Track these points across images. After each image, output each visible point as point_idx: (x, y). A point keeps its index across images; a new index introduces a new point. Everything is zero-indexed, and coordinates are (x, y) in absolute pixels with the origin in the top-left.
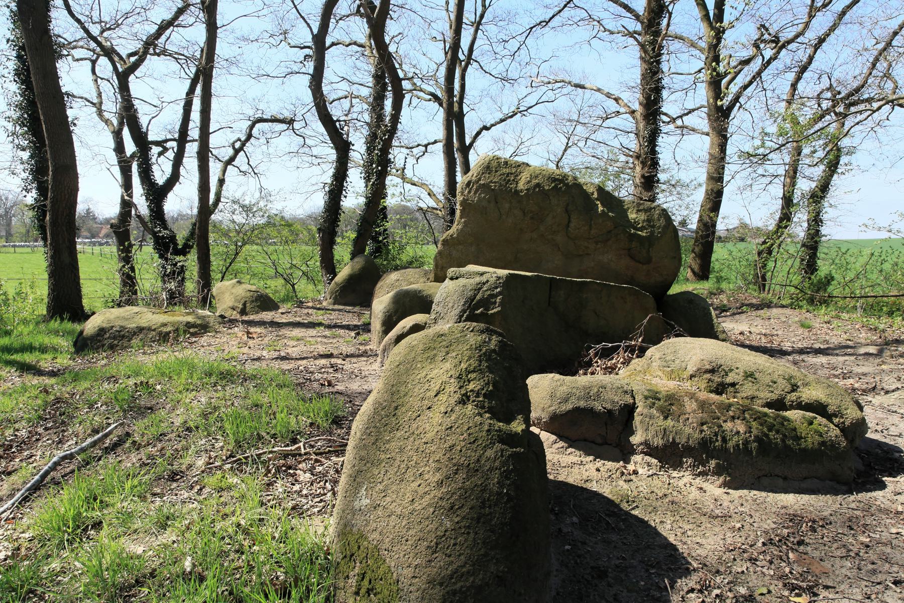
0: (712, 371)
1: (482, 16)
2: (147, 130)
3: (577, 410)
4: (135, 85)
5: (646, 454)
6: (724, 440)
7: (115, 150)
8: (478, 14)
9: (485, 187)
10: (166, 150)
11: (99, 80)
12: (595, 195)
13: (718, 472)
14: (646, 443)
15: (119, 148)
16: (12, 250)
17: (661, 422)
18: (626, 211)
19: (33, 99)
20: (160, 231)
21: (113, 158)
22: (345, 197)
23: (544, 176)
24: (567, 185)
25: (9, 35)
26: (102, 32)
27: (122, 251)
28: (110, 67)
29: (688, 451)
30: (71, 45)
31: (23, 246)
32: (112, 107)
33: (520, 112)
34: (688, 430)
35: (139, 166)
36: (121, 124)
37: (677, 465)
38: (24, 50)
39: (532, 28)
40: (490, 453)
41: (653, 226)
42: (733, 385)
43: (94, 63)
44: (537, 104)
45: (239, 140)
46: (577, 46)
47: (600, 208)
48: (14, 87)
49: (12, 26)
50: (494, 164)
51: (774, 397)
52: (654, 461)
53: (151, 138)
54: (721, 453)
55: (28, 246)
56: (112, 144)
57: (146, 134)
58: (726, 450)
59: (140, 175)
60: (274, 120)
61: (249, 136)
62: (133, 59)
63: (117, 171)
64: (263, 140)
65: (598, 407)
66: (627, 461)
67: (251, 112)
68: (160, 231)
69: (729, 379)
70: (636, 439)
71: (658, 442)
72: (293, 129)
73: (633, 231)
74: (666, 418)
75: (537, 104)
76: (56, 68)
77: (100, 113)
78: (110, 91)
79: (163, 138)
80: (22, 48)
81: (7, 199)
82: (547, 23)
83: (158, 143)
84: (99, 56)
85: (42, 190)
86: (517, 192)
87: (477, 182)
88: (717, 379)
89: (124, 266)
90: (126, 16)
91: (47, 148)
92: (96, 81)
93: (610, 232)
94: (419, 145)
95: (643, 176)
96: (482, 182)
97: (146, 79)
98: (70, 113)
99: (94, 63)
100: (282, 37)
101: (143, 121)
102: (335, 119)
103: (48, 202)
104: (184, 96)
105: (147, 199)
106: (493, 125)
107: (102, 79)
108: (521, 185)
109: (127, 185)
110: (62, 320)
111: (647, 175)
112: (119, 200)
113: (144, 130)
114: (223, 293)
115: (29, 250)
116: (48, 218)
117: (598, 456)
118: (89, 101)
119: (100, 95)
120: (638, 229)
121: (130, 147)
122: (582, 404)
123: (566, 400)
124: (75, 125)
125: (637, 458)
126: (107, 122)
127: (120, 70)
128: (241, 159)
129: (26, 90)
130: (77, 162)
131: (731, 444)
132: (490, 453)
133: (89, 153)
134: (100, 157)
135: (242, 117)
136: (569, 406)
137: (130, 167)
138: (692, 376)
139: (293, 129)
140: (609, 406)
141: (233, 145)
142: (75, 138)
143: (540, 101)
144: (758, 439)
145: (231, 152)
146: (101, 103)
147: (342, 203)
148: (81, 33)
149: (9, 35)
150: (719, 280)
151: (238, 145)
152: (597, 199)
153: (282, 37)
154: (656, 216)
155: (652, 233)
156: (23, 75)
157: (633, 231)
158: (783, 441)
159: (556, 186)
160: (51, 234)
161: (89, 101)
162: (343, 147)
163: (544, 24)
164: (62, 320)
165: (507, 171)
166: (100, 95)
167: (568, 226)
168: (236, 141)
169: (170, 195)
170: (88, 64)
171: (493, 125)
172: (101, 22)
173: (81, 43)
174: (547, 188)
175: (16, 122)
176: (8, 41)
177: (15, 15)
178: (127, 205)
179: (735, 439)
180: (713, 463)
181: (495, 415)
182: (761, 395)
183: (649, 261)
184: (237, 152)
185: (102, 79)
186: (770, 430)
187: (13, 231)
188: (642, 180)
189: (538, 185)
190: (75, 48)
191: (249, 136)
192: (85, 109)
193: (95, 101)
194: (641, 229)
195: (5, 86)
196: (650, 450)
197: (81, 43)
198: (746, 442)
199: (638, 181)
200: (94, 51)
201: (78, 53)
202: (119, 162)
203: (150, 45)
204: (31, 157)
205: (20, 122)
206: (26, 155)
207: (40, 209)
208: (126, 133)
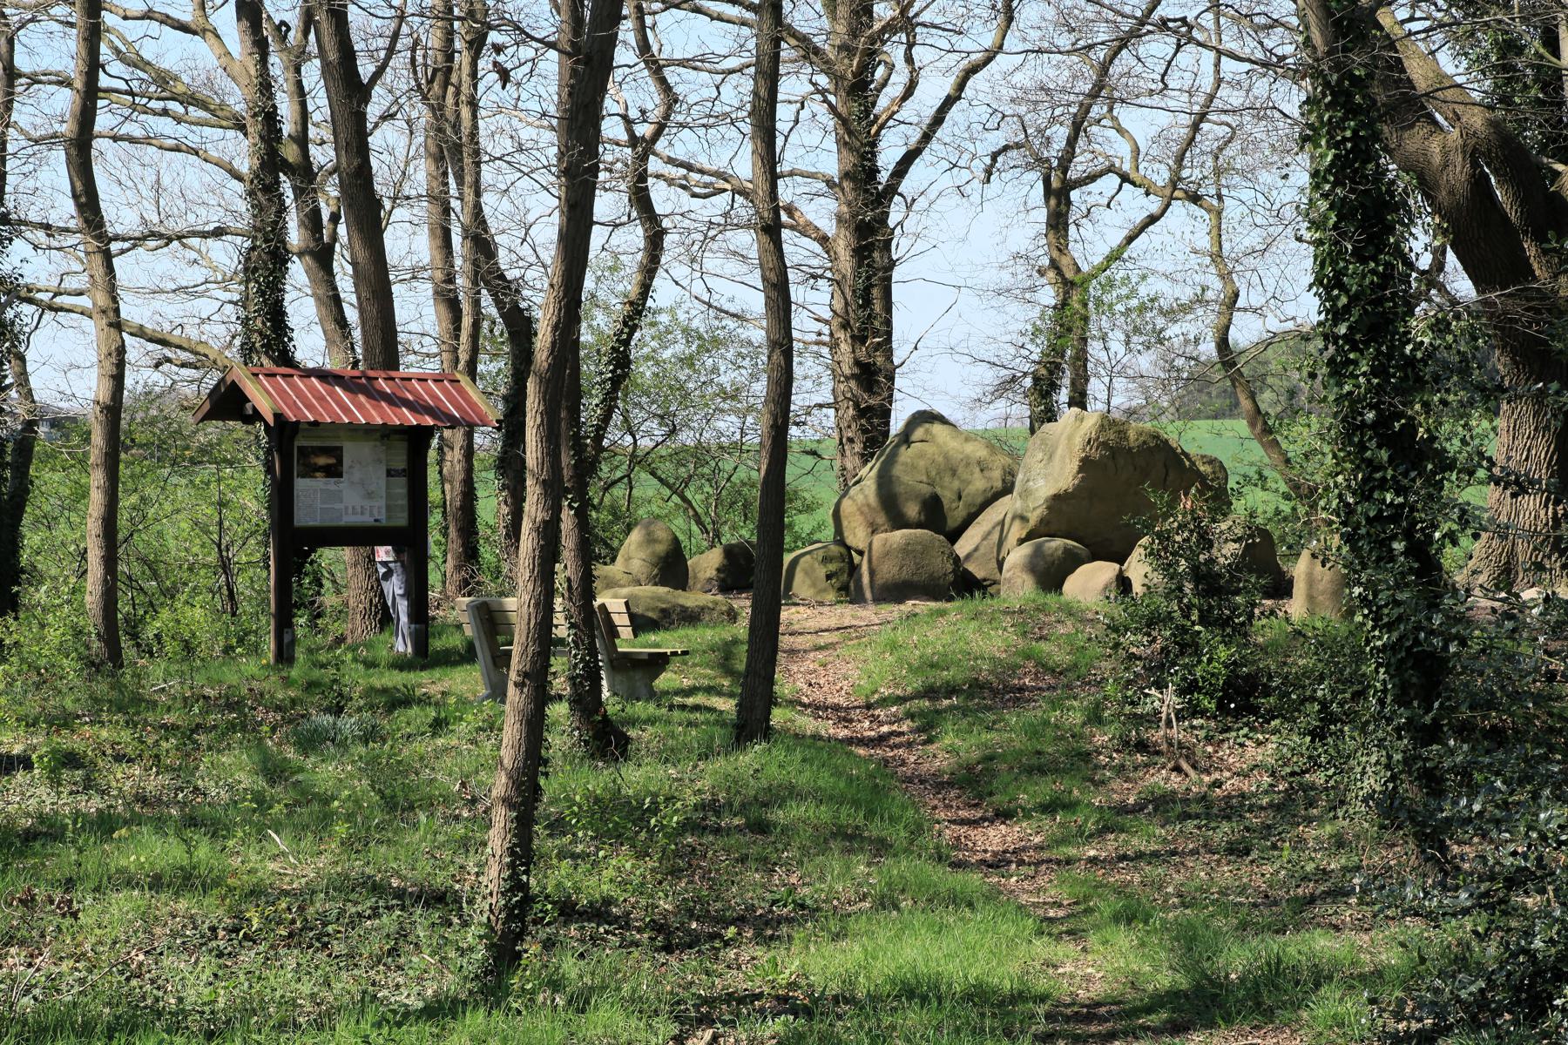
86: (1130, 449)
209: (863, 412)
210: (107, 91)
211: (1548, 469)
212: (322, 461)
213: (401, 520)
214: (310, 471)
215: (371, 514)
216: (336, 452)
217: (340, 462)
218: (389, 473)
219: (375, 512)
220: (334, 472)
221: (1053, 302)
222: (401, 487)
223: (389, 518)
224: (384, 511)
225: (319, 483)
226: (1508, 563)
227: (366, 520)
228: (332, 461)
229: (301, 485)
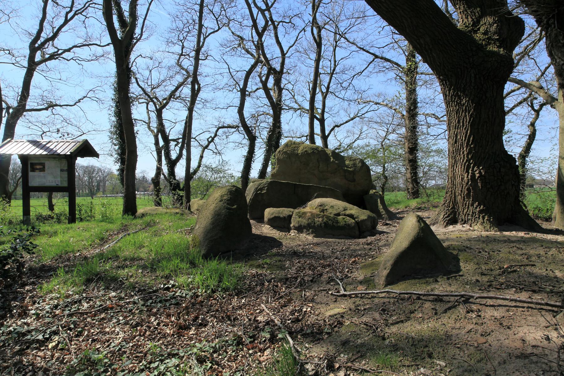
0: (321, 206)
1: (334, 70)
2: (169, 134)
3: (275, 217)
4: (166, 114)
5: (294, 229)
6: (314, 223)
7: (155, 144)
8: (332, 69)
9: (286, 153)
10: (178, 143)
11: (150, 112)
12: (331, 155)
13: (312, 233)
14: (294, 226)
15: (157, 143)
16: (106, 198)
17: (298, 219)
18: (345, 161)
19: (122, 124)
20: (173, 181)
21: (154, 148)
22: (254, 162)
23: (309, 147)
24: (318, 151)
25: (113, 97)
26: (152, 90)
27: (156, 191)
28: (154, 108)
29: (305, 227)
30: (137, 98)
31: (111, 196)
32: (154, 125)
33: (358, 117)
34: (305, 221)
35: (165, 151)
36: (158, 132)
37: (302, 232)
38: (119, 103)
39: (354, 76)
40: (223, 211)
41: (356, 166)
42: (326, 210)
43: (147, 104)
44: (367, 112)
45: (211, 137)
46: (389, 81)
47: (332, 159)
48: (114, 119)
49: (114, 93)
50: (290, 143)
51: (337, 212)
52: (296, 231)
53: (170, 138)
54: (313, 227)
55: (113, 196)
56: (153, 141)
57: (168, 136)
58: (315, 226)
59: (165, 155)
60: (229, 127)
61: (216, 135)
62: (165, 102)
63: (155, 154)
64: (224, 137)
65: (281, 216)
66: (289, 232)
67: (217, 124)
68: (173, 181)
69: (325, 208)
70: (292, 225)
71: (297, 225)
72: (238, 131)
73: (346, 168)
74: (299, 218)
75: (367, 112)
76: (131, 109)
77: (149, 127)
78: (153, 116)
79: (177, 137)
80: (117, 102)
81: (104, 172)
82: (361, 73)
83: (174, 140)
84: (149, 102)
85: (123, 163)
86: (298, 154)
87: (282, 151)
88: (322, 208)
89: (156, 198)
90: (163, 81)
91: (126, 144)
92: (148, 112)
93: (336, 169)
94: (303, 136)
95: (409, 148)
96: (284, 151)
97: (171, 110)
98: (136, 129)
99: (147, 104)
100: (234, 87)
101: (167, 131)
102: (249, 126)
103: (125, 166)
104: (185, 118)
105: (167, 166)
106: (341, 125)
107: (151, 111)
108: (299, 152)
109: (159, 160)
110: (128, 215)
111: (411, 147)
112: (156, 168)
113: (168, 134)
114: (194, 204)
115: (114, 198)
116: (125, 173)
117: (281, 231)
118: (144, 122)
119: (149, 118)
120: (349, 168)
121: (161, 143)
122: (277, 215)
123: (272, 214)
124: (137, 134)
125: (292, 231)
126: (152, 131)
127: (158, 108)
128: (212, 146)
129: (118, 120)
130: (137, 150)
131: (316, 224)
132: (223, 211)
133: (143, 146)
134: (148, 148)
135: (213, 126)
136: (273, 216)
137: (161, 152)
138: (316, 208)
139: (238, 131)
140: (284, 216)
141: (208, 139)
142: (137, 139)
143: (369, 110)
144: (325, 223)
145: (207, 143)
146: (150, 122)
147: (252, 165)
148: (142, 92)
149: (113, 97)
150: (428, 196)
151: (210, 140)
152: (331, 156)
153: (234, 87)
154: (358, 162)
155: (355, 169)
156: (118, 114)
157: (346, 168)
158: (332, 223)
159: (313, 151)
160: (126, 179)
161: (144, 122)
162: (252, 139)
163: (360, 74)
164: (128, 215)
165: (295, 146)
166: (149, 118)
167: (319, 167)
168: (209, 138)
169: (178, 164)
170: (145, 105)
171: (341, 125)
172: (152, 85)
173: (142, 97)
174: (309, 152)
175: (111, 132)
176: (112, 99)
177: (116, 89)
178: (159, 170)
179: (318, 223)
180: (311, 230)
181: (228, 204)
182: (333, 212)
183: (354, 181)
184: (209, 143)
185: (151, 111)
186: (329, 220)
187: (106, 189)
188: (409, 150)
189: (306, 151)
190: (140, 98)
191: (216, 135)
192: (142, 126)
193: (147, 122)
194: (350, 168)
195: (110, 118)
196: (295, 228)
197: (142, 97)
198: (321, 224)
199: (406, 150)
200: (147, 100)
201: (141, 101)
202: (156, 149)
203: (172, 95)
204: (119, 148)
205: (115, 133)
206: (117, 147)
207: (121, 170)
208: (160, 136)
209: (410, 161)
210: (284, 109)
211: (467, 147)
212: (38, 167)
213: (65, 184)
214: (33, 170)
215: (55, 183)
216: (43, 165)
217: (44, 167)
218: (62, 170)
219: (57, 182)
220: (43, 170)
221: (529, 133)
222: (65, 175)
223: (61, 184)
224: (60, 182)
225: (37, 173)
226: (453, 208)
227: (54, 184)
228: (41, 167)
229: (31, 174)
